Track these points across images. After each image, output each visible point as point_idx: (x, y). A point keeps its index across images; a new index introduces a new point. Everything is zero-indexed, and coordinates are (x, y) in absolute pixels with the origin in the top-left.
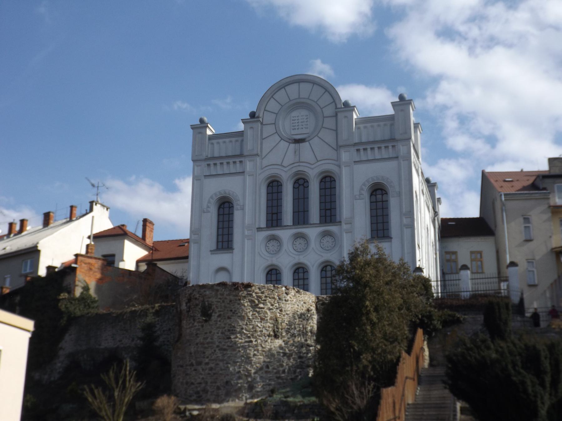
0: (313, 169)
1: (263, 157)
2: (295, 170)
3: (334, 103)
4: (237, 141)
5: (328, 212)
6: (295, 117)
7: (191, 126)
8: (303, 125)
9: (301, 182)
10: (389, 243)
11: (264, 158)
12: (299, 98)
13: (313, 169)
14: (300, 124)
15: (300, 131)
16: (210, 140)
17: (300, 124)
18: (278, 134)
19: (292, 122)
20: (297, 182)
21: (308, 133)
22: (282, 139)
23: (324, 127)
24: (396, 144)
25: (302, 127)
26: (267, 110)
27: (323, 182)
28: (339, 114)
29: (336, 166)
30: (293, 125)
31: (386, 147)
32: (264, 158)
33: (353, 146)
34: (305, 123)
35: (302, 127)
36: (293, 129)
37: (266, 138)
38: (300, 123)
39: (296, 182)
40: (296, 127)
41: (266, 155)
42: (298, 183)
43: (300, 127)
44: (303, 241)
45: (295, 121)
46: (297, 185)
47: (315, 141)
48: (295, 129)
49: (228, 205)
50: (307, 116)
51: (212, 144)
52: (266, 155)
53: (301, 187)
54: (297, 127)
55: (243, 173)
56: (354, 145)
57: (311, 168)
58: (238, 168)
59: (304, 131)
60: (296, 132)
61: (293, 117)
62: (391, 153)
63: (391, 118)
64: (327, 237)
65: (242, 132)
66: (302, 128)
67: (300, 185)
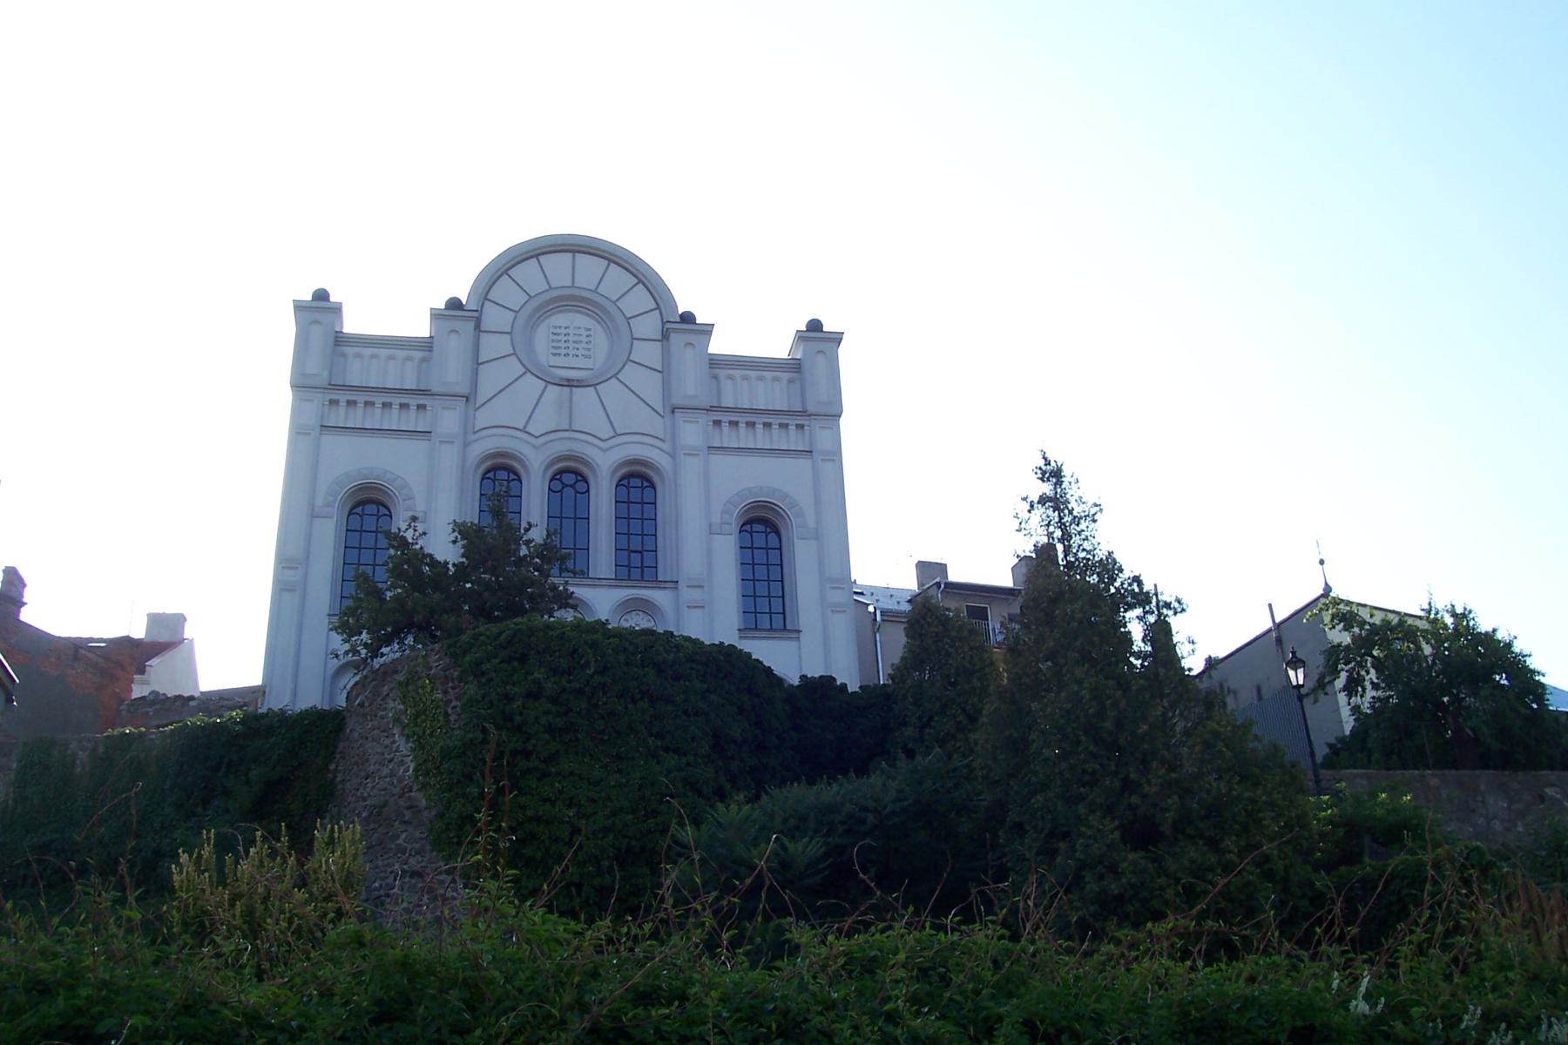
0: (604, 450)
1: (477, 406)
2: (560, 448)
3: (658, 311)
4: (409, 359)
5: (636, 558)
6: (560, 327)
7: (431, 309)
8: (578, 349)
9: (569, 479)
10: (794, 644)
11: (479, 407)
12: (595, 291)
13: (604, 450)
14: (571, 345)
15: (571, 362)
16: (339, 345)
17: (571, 345)
18: (517, 357)
19: (552, 337)
20: (558, 477)
21: (592, 369)
22: (528, 370)
23: (631, 361)
24: (806, 423)
25: (576, 352)
26: (492, 299)
27: (624, 485)
28: (673, 337)
29: (669, 458)
30: (554, 344)
31: (767, 425)
32: (479, 407)
33: (705, 412)
34: (584, 345)
35: (576, 352)
36: (555, 354)
37: (487, 362)
38: (571, 342)
39: (557, 476)
40: (563, 352)
41: (483, 404)
42: (560, 480)
43: (571, 352)
44: (645, 620)
45: (558, 338)
46: (557, 486)
47: (611, 389)
48: (559, 354)
49: (376, 509)
50: (590, 330)
51: (715, 377)
52: (483, 404)
53: (569, 492)
54: (565, 352)
55: (429, 434)
56: (707, 410)
57: (599, 448)
58: (410, 421)
59: (581, 363)
60: (560, 361)
61: (556, 327)
62: (793, 440)
63: (426, 345)
64: (637, 614)
65: (798, 362)
66: (577, 356)
67: (564, 486)
